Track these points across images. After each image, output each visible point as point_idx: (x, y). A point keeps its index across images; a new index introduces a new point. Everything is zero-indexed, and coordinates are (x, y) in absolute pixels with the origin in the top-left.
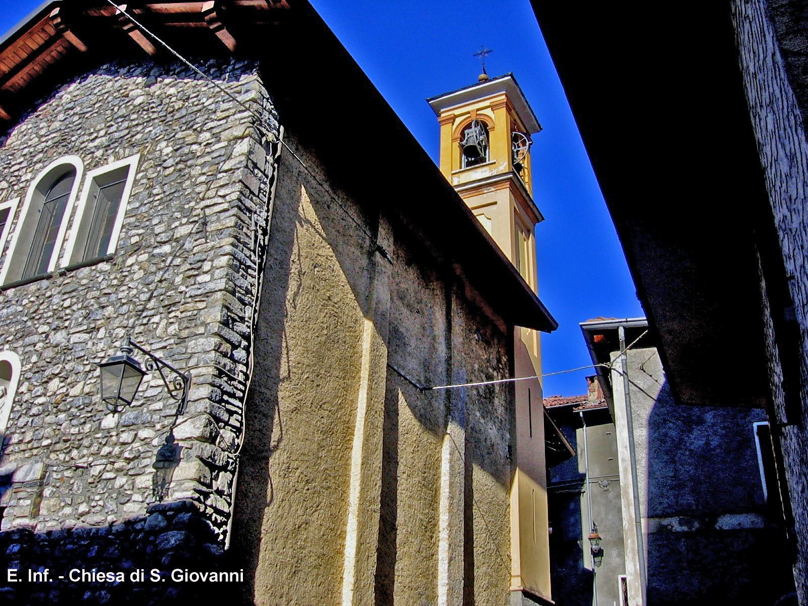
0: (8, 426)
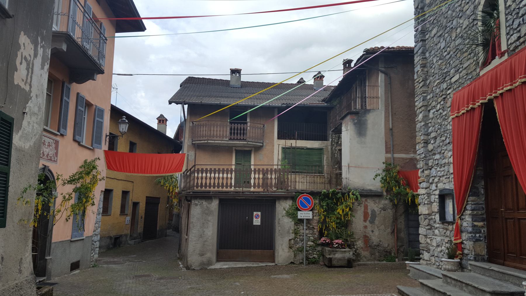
0: (507, 32)
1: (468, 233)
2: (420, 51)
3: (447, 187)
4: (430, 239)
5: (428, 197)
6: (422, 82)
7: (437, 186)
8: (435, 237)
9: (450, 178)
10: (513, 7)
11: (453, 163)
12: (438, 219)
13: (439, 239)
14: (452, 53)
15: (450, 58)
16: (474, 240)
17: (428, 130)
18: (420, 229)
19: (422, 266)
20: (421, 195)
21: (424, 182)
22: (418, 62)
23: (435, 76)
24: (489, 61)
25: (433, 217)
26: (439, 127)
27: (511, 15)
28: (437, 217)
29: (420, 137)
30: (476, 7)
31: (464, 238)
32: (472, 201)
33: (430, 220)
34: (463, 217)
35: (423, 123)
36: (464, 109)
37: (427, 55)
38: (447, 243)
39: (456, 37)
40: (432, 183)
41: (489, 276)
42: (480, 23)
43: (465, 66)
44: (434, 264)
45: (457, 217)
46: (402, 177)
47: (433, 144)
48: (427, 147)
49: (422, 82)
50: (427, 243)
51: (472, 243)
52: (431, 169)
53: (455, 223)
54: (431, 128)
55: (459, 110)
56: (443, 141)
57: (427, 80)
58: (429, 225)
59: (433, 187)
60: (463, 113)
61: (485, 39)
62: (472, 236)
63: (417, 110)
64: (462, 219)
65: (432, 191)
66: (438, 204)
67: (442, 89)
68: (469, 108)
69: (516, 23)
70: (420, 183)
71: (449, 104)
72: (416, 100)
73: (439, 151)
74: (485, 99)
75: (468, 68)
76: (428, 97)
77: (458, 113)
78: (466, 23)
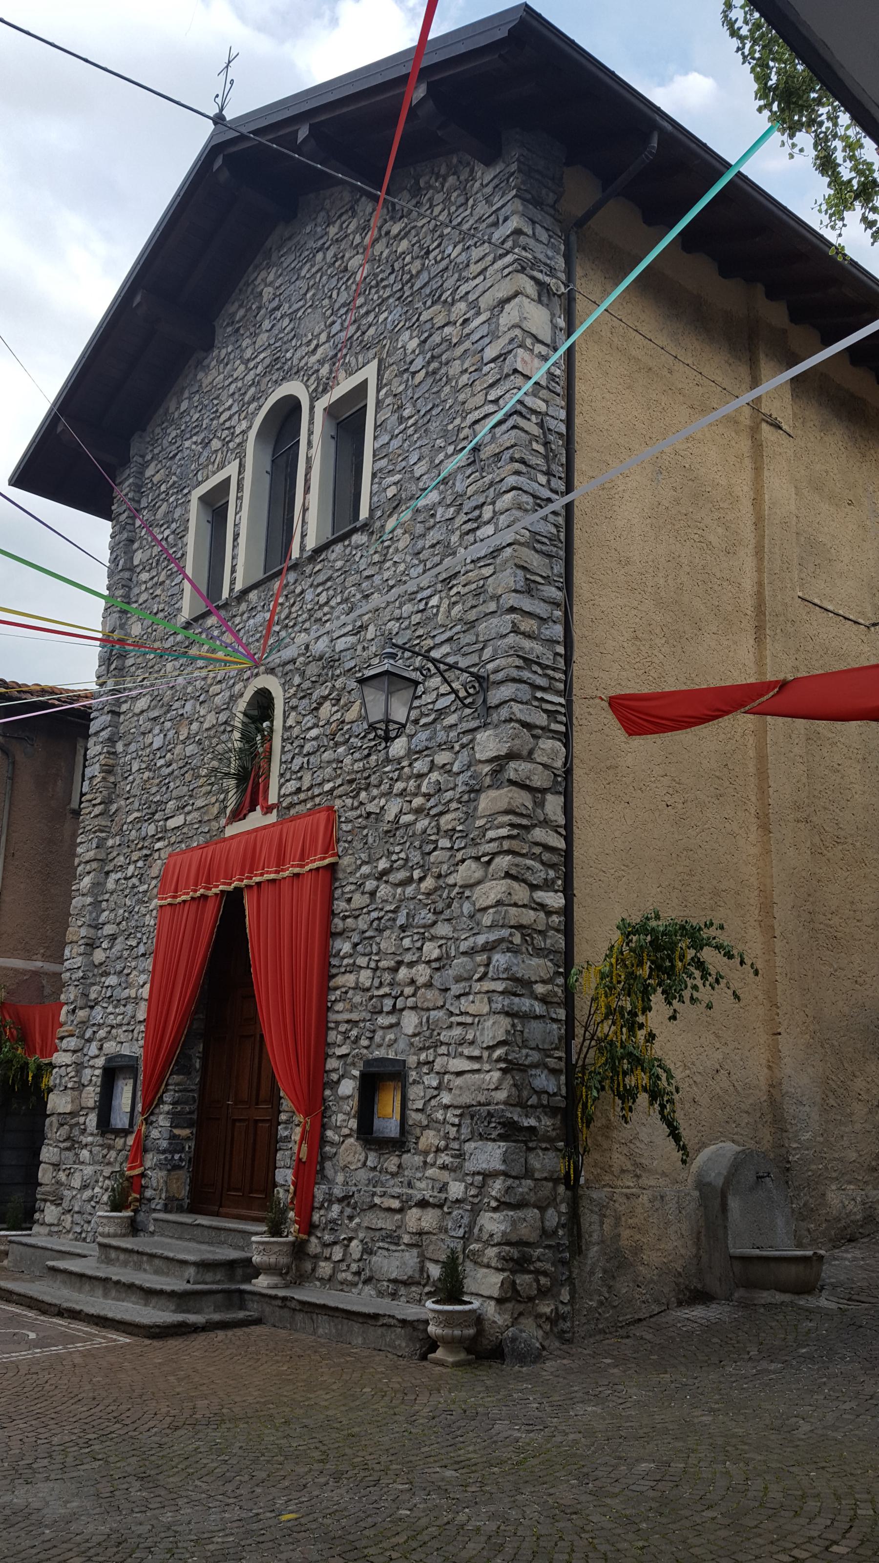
1: (160, 1152)
2: (105, 734)
3: (126, 1050)
4: (67, 1172)
5: (77, 1072)
6: (100, 804)
7: (101, 1048)
8: (81, 1167)
9: (136, 1032)
10: (296, 731)
11: (149, 1000)
12: (94, 1124)
13: (89, 1170)
14: (174, 766)
15: (170, 774)
16: (169, 1167)
17: (98, 916)
18: (44, 1149)
19: (38, 1236)
20: (60, 1067)
21: (72, 1036)
22: (95, 756)
23: (131, 800)
24: (245, 812)
25: (82, 1120)
26: (126, 914)
27: (292, 743)
28: (92, 1120)
29: (78, 930)
30: (233, 698)
31: (148, 1164)
32: (176, 1084)
33: (72, 1127)
34: (153, 1118)
35: (89, 900)
36: (188, 894)
37: (120, 747)
38: (109, 1178)
39: (188, 738)
40: (89, 1041)
41: (190, 1240)
42: (237, 735)
43: (199, 803)
44: (68, 1232)
45: (139, 1119)
46: (8, 1020)
47: (105, 949)
48: (91, 954)
49: (100, 804)
50: (57, 1182)
51: (164, 1173)
52: (92, 1007)
53: (132, 1132)
54: (106, 913)
55: (176, 891)
56: (132, 948)
57: (111, 802)
58: (68, 1138)
59: (93, 1049)
60: (184, 901)
61: (244, 768)
62: (166, 1158)
63: (79, 865)
64: (148, 1122)
65: (87, 1058)
66: (98, 1090)
67: (143, 834)
68: (198, 894)
69: (298, 761)
70: (62, 1038)
71: (154, 872)
72: (79, 840)
73: (118, 968)
74: (230, 884)
75: (203, 810)
76: (110, 842)
77: (174, 897)
78: (210, 720)
